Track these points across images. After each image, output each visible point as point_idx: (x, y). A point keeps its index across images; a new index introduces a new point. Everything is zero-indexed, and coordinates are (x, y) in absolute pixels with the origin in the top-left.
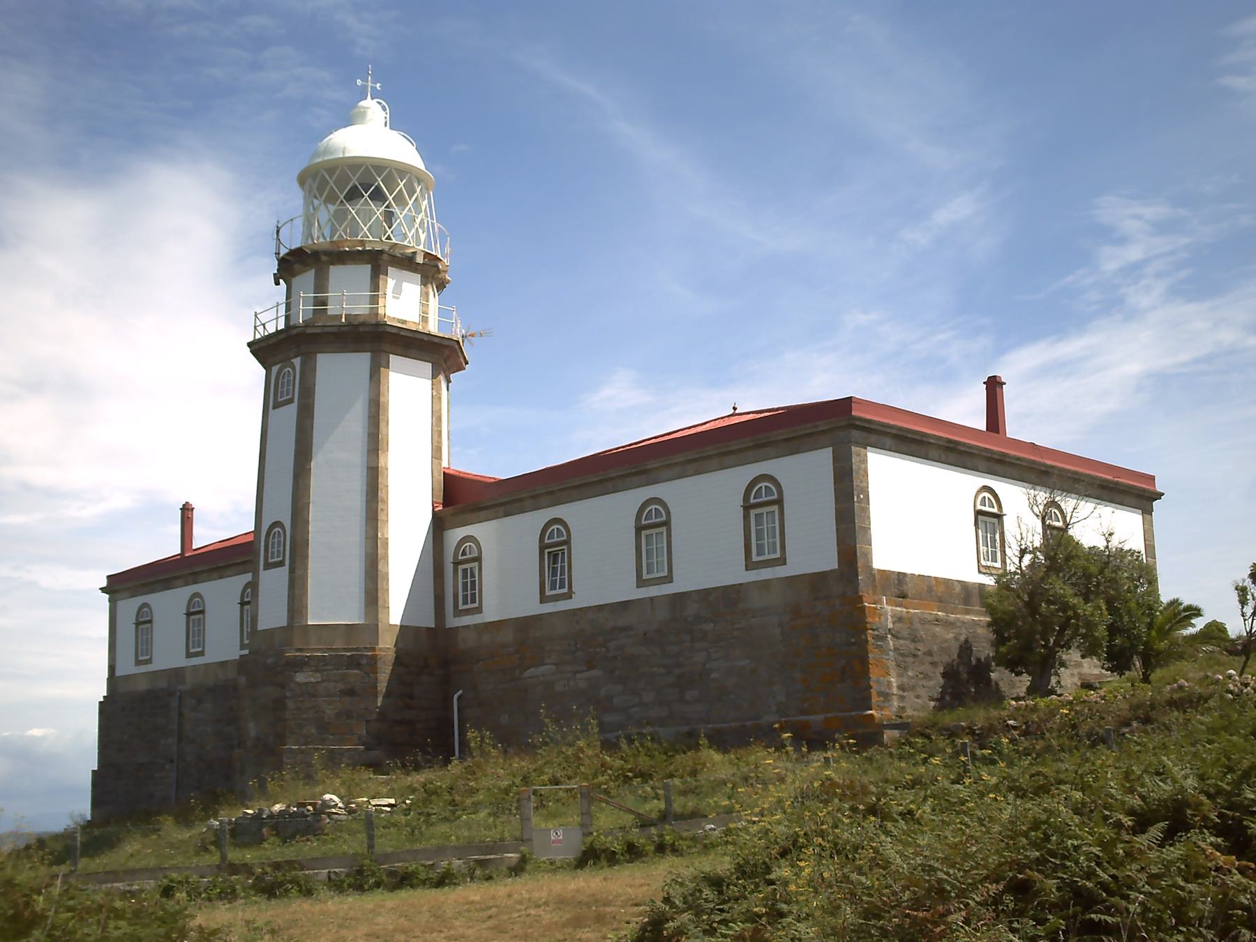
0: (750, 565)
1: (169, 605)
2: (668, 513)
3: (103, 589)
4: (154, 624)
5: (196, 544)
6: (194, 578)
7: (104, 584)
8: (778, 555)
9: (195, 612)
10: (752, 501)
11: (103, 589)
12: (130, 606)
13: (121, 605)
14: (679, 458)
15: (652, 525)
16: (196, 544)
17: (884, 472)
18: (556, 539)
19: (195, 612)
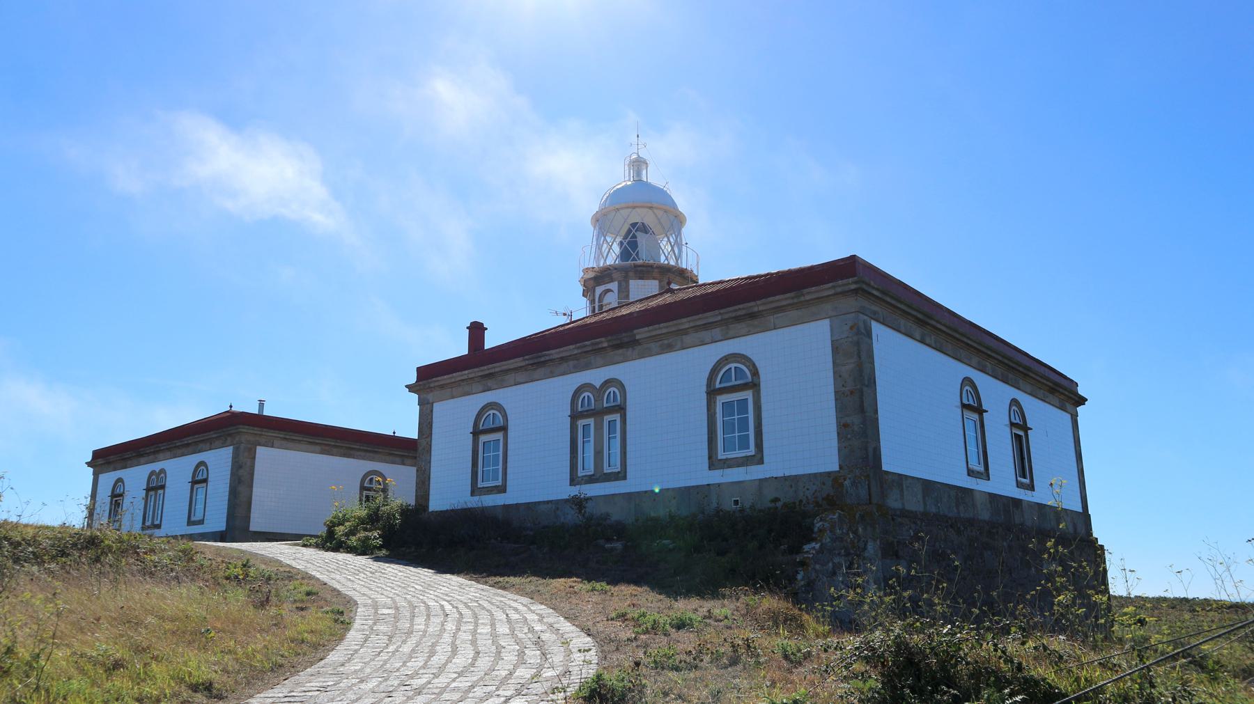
0: (714, 463)
1: (135, 477)
2: (755, 373)
3: (410, 388)
4: (167, 490)
5: (489, 344)
6: (490, 381)
7: (89, 459)
8: (499, 483)
9: (155, 487)
10: (718, 385)
11: (410, 388)
12: (108, 479)
13: (102, 477)
14: (190, 440)
15: (599, 411)
16: (489, 344)
17: (895, 353)
18: (734, 383)
19: (155, 487)
